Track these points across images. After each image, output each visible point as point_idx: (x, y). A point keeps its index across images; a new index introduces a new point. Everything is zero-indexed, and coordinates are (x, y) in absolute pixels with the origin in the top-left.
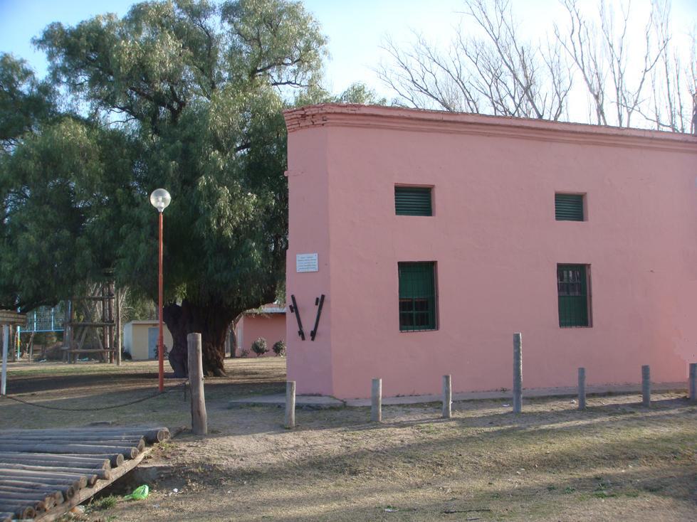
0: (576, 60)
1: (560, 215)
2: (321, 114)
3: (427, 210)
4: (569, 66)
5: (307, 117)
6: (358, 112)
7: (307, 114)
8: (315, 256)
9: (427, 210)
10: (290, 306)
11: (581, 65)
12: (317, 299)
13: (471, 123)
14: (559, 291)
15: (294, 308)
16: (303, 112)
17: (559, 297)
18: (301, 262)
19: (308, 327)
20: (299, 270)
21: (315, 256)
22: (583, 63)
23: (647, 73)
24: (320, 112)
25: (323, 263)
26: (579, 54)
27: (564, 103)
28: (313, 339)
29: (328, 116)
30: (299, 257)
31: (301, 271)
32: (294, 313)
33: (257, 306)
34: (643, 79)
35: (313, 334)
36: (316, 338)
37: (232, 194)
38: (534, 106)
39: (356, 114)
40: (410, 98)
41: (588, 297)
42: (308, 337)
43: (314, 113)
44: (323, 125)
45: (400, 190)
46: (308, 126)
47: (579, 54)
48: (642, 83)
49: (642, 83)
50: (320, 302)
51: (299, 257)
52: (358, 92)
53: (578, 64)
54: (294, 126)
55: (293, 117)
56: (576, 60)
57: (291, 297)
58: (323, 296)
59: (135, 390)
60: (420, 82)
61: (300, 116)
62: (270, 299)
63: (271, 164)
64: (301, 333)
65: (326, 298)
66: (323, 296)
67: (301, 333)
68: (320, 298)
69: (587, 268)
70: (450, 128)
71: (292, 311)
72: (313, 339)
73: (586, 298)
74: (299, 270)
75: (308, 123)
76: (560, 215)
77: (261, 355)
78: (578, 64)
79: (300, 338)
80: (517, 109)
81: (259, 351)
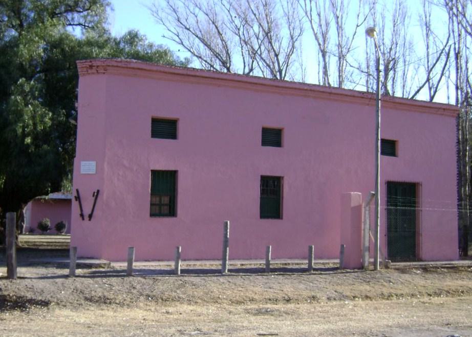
0: (306, 13)
1: (265, 143)
2: (103, 66)
3: (173, 135)
4: (301, 18)
5: (93, 68)
6: (129, 66)
7: (93, 65)
8: (93, 163)
9: (173, 135)
10: (75, 197)
11: (310, 18)
12: (94, 193)
13: (206, 77)
14: (261, 194)
15: (78, 198)
16: (90, 64)
17: (261, 198)
18: (84, 166)
19: (87, 211)
20: (82, 172)
21: (93, 163)
22: (311, 16)
23: (358, 28)
24: (103, 64)
25: (99, 168)
26: (308, 9)
27: (296, 44)
28: (90, 220)
29: (108, 68)
30: (83, 163)
31: (84, 173)
32: (78, 202)
33: (47, 194)
34: (355, 32)
35: (90, 216)
36: (92, 219)
37: (34, 111)
38: (273, 48)
39: (127, 68)
40: (176, 33)
41: (281, 199)
42: (86, 218)
43: (98, 64)
44: (104, 73)
45: (155, 121)
46: (93, 73)
47: (308, 9)
48: (354, 35)
49: (354, 35)
50: (97, 195)
51: (83, 163)
52: (133, 38)
53: (307, 16)
54: (83, 73)
55: (84, 66)
56: (306, 13)
57: (76, 191)
58: (98, 191)
59: (378, 146)
60: (183, 21)
61: (88, 66)
62: (57, 188)
63: (42, 7)
64: (82, 215)
65: (100, 193)
66: (98, 191)
67: (82, 215)
68: (96, 191)
69: (281, 179)
70: (192, 79)
71: (76, 200)
72: (90, 220)
73: (280, 199)
74: (82, 172)
75: (94, 71)
76: (265, 143)
77: (45, 232)
78: (307, 16)
79: (81, 219)
80: (260, 47)
81: (43, 229)
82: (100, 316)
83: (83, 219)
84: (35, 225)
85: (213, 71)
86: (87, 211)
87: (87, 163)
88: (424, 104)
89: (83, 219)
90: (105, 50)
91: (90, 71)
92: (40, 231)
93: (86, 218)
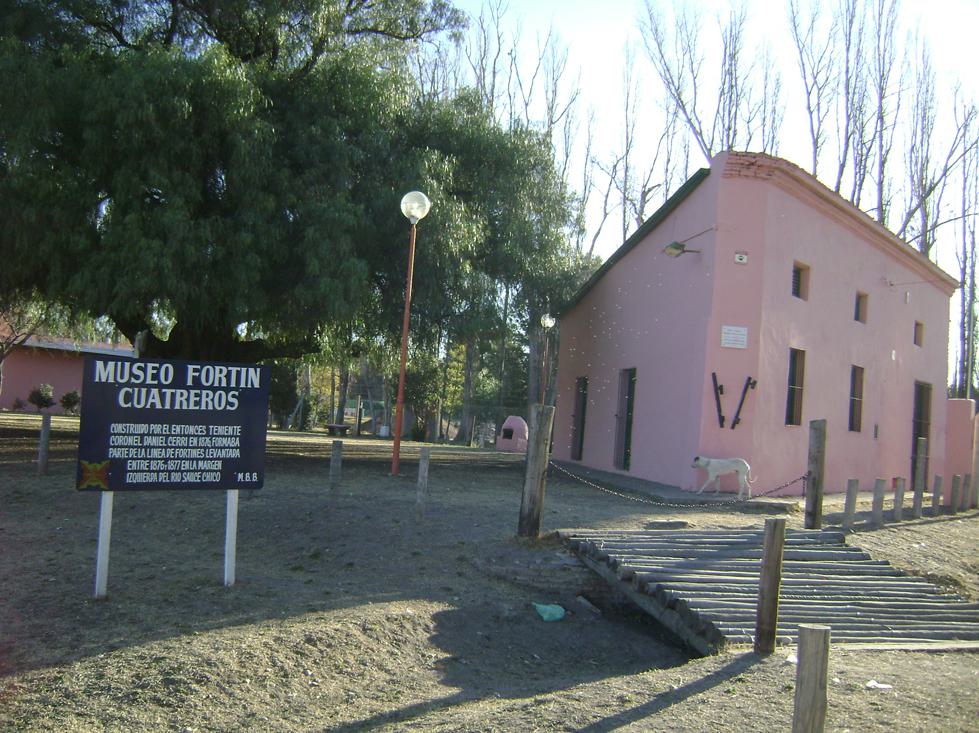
8: (744, 331)
21: (744, 331)
25: (753, 340)
34: (580, 74)
35: (736, 421)
50: (750, 383)
64: (722, 420)
67: (722, 420)
75: (750, 172)
82: (204, 533)
83: (722, 426)
84: (25, 396)
85: (350, 118)
86: (729, 413)
87: (733, 328)
88: (822, 191)
89: (722, 426)
90: (109, 77)
91: (744, 172)
92: (35, 407)
93: (728, 423)
